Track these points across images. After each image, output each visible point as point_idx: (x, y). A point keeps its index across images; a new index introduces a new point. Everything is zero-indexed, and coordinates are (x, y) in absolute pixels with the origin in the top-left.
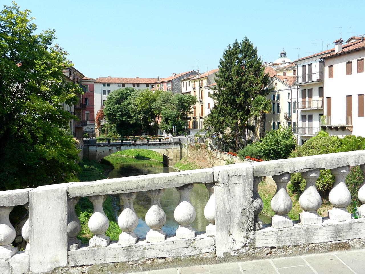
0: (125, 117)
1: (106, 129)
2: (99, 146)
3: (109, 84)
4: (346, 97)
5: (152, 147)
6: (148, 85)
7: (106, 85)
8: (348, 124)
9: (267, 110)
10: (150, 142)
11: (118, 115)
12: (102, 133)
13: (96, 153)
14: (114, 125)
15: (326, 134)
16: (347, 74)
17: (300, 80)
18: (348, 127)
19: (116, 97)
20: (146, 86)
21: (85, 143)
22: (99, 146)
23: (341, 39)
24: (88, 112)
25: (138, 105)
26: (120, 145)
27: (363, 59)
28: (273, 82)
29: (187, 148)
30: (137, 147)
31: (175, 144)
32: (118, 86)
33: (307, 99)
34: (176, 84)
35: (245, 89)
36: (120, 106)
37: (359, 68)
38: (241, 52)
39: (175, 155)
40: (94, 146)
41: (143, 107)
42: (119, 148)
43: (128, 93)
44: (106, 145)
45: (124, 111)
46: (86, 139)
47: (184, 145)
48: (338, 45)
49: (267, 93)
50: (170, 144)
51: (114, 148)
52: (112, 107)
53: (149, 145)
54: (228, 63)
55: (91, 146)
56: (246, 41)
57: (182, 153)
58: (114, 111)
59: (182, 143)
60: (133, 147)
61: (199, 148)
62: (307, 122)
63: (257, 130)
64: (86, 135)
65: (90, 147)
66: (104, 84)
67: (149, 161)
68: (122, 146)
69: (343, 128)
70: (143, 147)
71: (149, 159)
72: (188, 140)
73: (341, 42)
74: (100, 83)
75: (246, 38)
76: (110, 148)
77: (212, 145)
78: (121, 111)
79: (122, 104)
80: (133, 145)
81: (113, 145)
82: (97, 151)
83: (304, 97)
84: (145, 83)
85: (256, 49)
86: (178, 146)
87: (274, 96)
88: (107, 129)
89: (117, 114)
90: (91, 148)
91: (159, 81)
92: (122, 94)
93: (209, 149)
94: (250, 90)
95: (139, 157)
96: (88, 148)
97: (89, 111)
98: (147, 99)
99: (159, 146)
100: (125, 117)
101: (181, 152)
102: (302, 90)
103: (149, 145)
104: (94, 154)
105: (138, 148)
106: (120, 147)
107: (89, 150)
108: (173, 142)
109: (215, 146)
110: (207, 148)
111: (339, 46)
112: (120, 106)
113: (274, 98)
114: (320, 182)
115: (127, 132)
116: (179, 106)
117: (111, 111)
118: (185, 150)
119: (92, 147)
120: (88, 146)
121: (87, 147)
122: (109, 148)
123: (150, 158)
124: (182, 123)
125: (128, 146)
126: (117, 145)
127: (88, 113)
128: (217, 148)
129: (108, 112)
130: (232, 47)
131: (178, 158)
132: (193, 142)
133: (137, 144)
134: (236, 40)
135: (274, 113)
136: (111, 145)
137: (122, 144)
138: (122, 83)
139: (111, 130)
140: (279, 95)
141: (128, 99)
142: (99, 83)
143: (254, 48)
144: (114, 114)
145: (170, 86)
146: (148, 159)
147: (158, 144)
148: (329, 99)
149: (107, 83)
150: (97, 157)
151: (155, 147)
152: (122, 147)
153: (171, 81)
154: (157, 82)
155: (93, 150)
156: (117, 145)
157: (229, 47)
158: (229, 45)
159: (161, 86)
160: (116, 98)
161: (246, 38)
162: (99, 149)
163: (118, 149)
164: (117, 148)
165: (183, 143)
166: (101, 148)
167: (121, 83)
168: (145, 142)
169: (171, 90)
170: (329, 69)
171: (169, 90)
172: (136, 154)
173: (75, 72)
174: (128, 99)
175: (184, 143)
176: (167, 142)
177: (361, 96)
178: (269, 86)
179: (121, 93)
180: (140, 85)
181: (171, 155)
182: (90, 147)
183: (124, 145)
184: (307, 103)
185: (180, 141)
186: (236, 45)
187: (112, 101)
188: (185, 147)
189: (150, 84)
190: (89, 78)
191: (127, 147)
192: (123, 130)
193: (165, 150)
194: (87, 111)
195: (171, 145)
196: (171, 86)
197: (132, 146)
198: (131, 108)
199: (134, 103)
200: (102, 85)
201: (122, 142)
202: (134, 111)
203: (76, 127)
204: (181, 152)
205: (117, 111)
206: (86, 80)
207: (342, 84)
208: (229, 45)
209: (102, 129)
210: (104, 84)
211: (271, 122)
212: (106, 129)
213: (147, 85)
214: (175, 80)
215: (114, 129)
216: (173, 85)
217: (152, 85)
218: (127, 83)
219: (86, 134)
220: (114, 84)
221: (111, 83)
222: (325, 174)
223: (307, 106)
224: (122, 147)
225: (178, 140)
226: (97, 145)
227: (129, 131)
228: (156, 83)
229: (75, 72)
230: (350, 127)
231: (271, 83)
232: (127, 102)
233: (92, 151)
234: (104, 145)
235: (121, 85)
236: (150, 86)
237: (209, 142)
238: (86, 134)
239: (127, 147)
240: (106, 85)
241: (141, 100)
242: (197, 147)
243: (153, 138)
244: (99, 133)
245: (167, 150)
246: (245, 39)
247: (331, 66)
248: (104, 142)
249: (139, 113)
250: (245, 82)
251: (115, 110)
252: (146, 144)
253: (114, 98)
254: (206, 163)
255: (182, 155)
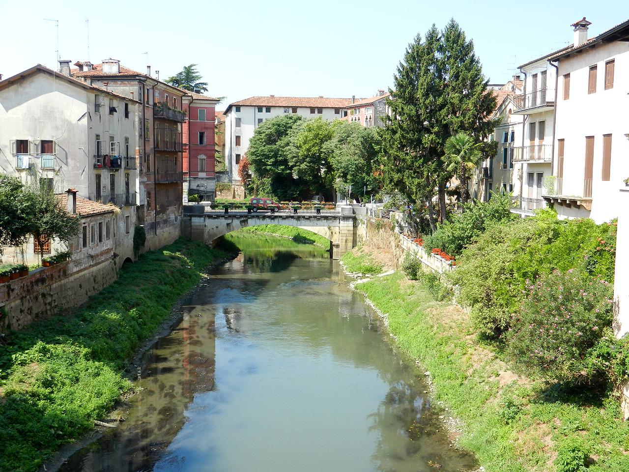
0: (281, 167)
1: (255, 186)
2: (210, 217)
3: (268, 109)
4: (603, 137)
5: (303, 221)
6: (337, 110)
7: (264, 109)
8: (586, 193)
9: (471, 161)
10: (301, 212)
11: (269, 164)
12: (250, 194)
13: (203, 230)
14: (267, 180)
15: (553, 212)
16: (590, 92)
17: (529, 104)
18: (582, 201)
19: (268, 132)
20: (334, 112)
21: (185, 212)
22: (210, 217)
23: (585, 18)
24: (204, 157)
25: (300, 147)
26: (246, 216)
27: (613, 61)
28: (505, 108)
29: (365, 226)
30: (276, 220)
31: (346, 218)
32: (285, 112)
33: (537, 140)
34: (380, 109)
35: (442, 120)
36: (274, 147)
37: (608, 78)
38: (441, 49)
39: (344, 238)
40: (200, 216)
41: (309, 150)
42: (244, 222)
43: (288, 124)
44: (222, 216)
45: (280, 157)
46: (191, 205)
47: (362, 220)
48: (578, 32)
49: (488, 129)
50: (335, 218)
51: (236, 222)
52: (260, 149)
53: (298, 218)
54: (412, 69)
55: (195, 216)
56: (453, 27)
57: (357, 236)
58: (263, 155)
59: (357, 216)
60: (270, 220)
61: (382, 228)
62: (535, 186)
63: (480, 199)
64: (195, 198)
65: (194, 218)
66: (260, 109)
67: (313, 246)
68: (249, 218)
69: (572, 204)
70: (287, 221)
71: (312, 242)
72: (367, 213)
73: (584, 26)
74: (254, 106)
75: (452, 21)
76: (229, 221)
77: (402, 223)
78: (275, 156)
79: (277, 143)
80: (269, 217)
81: (234, 216)
82: (205, 226)
83: (532, 138)
84: (333, 108)
85: (471, 44)
86: (351, 223)
87: (507, 134)
88: (257, 187)
89: (268, 161)
90: (196, 221)
91: (354, 105)
92: (279, 125)
93: (397, 229)
94: (451, 121)
95: (299, 239)
96: (191, 220)
97: (206, 155)
98: (317, 136)
99: (316, 222)
100: (281, 167)
101: (355, 234)
102: (531, 124)
103: (298, 218)
104: (201, 232)
105: (278, 223)
106: (247, 220)
107: (192, 224)
108: (340, 215)
109: (407, 225)
110: (393, 229)
111: (580, 35)
112: (274, 147)
113: (506, 140)
114: (504, 312)
115: (285, 194)
116: (363, 150)
117: (258, 156)
118: (362, 230)
119: (196, 218)
120: (191, 216)
121: (189, 218)
122: (226, 221)
123: (314, 242)
124: (369, 180)
125: (261, 220)
126: (241, 216)
127: (204, 159)
128: (410, 230)
129: (254, 157)
130: (423, 41)
131: (350, 244)
132: (374, 216)
133: (276, 217)
134: (434, 25)
135: (505, 167)
136: (230, 216)
137: (227, 215)
138: (292, 107)
139: (264, 189)
140: (513, 133)
141: (287, 134)
142: (252, 106)
143: (467, 41)
144: (263, 160)
145: (370, 112)
146: (311, 243)
147: (315, 217)
148: (562, 141)
149: (265, 106)
150: (206, 236)
151: (308, 222)
152: (249, 221)
153: (372, 104)
154: (350, 105)
155: (198, 224)
156: (241, 216)
157: (418, 39)
158: (419, 35)
159: (356, 113)
160: (267, 133)
161: (452, 21)
162: (210, 224)
163: (243, 224)
164: (241, 222)
165: (359, 217)
166: (213, 220)
167: (290, 107)
168: (313, 212)
169: (371, 120)
170: (565, 80)
171: (354, 121)
172: (294, 233)
173: (156, 85)
174: (287, 134)
175: (361, 218)
176: (330, 215)
177: (608, 136)
178: (500, 114)
179: (277, 125)
180: (324, 111)
181: (337, 239)
182: (193, 218)
183: (253, 217)
184: (536, 148)
185: (354, 213)
186: (432, 37)
187: (262, 139)
188: (363, 225)
189: (341, 110)
190: (212, 97)
191: (258, 220)
192: (278, 190)
193: (326, 228)
194: (201, 156)
195: (338, 220)
196: (372, 112)
197: (268, 220)
198: (290, 152)
199: (295, 144)
200: (257, 110)
201: (226, 211)
202: (294, 157)
203: (157, 182)
204: (355, 234)
205: (268, 157)
206: (203, 100)
207: (584, 109)
208: (419, 35)
209: (250, 186)
210: (260, 109)
211: (500, 185)
212: (255, 186)
213: (293, 109)
214: (379, 102)
215: (268, 188)
216: (376, 111)
217: (346, 110)
218: (301, 107)
219: (196, 196)
220: (277, 108)
221: (298, 107)
222: (514, 296)
223: (536, 155)
224: (249, 221)
225: (350, 211)
226: (205, 215)
227: (288, 192)
228: (351, 108)
229: (156, 85)
230: (586, 201)
231: (504, 110)
232: (285, 140)
233: (196, 226)
234: (218, 217)
235: (291, 110)
236: (342, 112)
237: (397, 217)
238: (196, 196)
239: (258, 221)
240: (264, 109)
241: (306, 137)
242: (378, 227)
243: (305, 206)
244: (245, 193)
245: (329, 228)
246: (451, 23)
247: (567, 76)
248: (241, 211)
249: (304, 160)
250: (442, 106)
251: (265, 154)
252: (292, 217)
253: (264, 132)
254: (390, 256)
255: (358, 240)
